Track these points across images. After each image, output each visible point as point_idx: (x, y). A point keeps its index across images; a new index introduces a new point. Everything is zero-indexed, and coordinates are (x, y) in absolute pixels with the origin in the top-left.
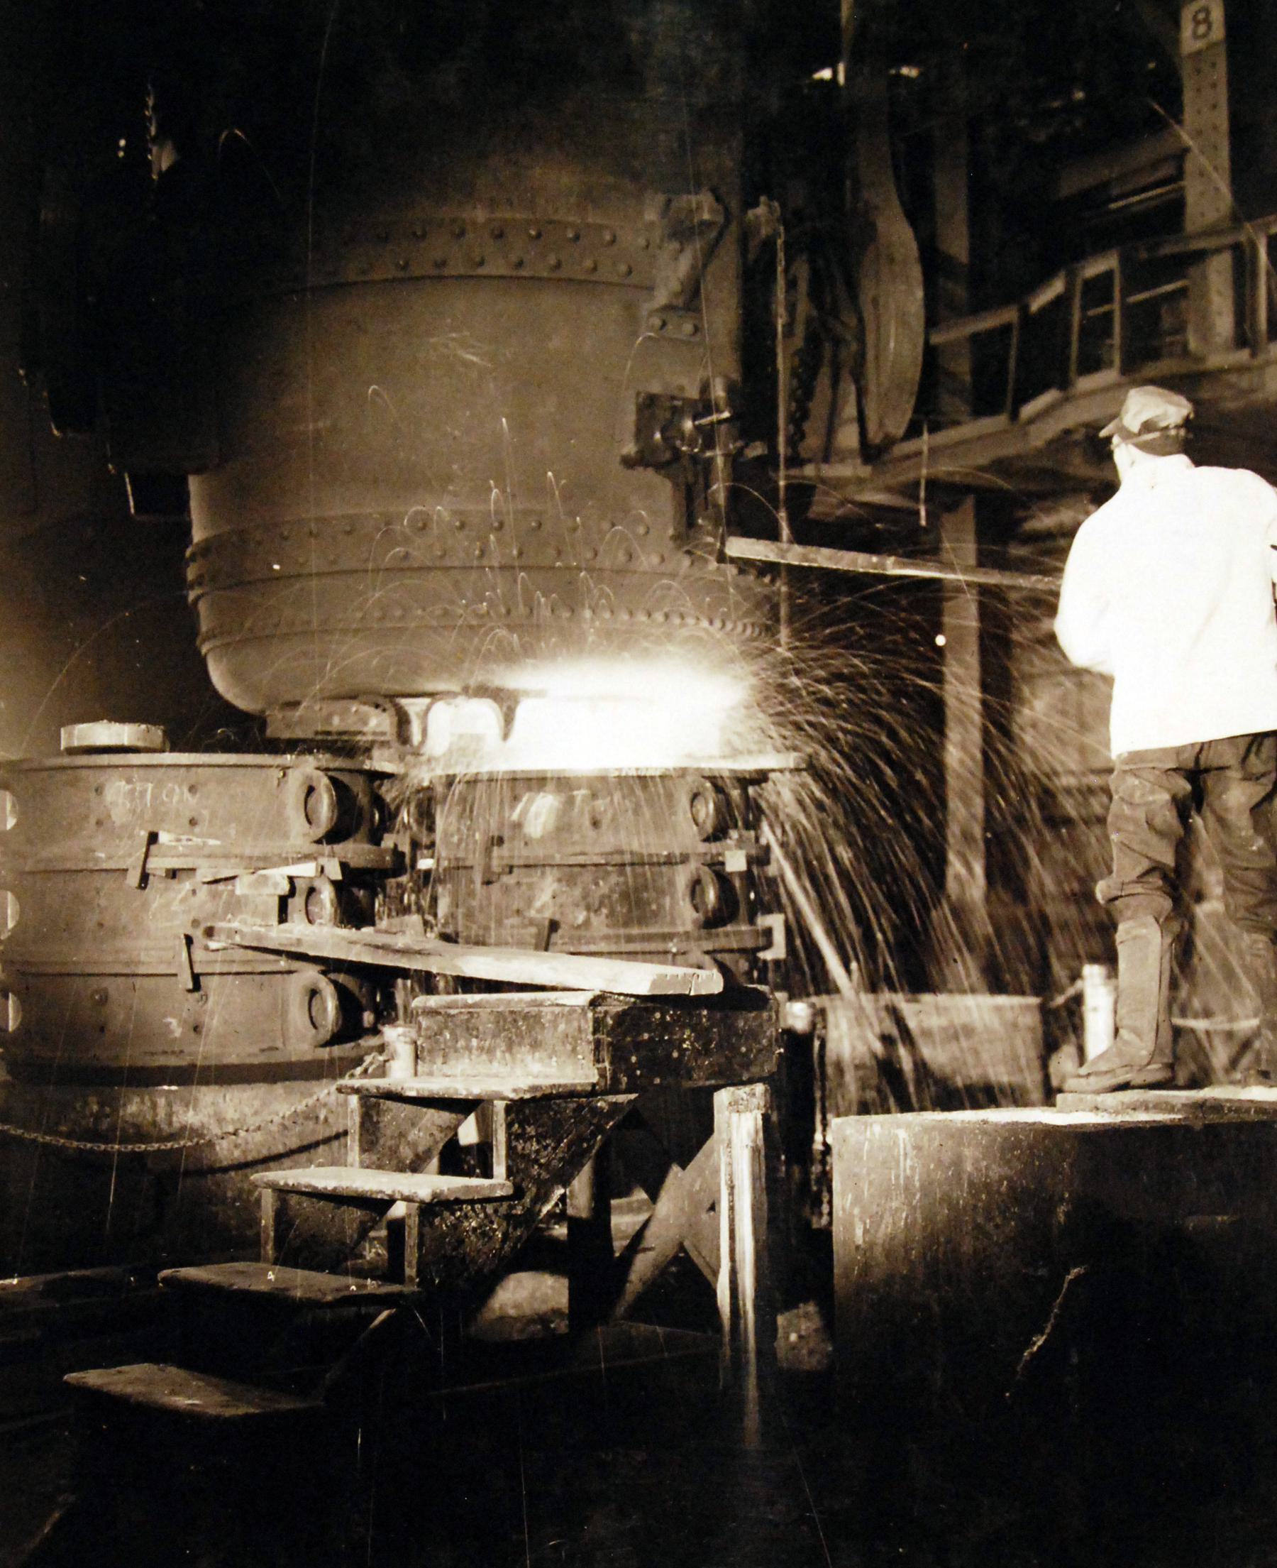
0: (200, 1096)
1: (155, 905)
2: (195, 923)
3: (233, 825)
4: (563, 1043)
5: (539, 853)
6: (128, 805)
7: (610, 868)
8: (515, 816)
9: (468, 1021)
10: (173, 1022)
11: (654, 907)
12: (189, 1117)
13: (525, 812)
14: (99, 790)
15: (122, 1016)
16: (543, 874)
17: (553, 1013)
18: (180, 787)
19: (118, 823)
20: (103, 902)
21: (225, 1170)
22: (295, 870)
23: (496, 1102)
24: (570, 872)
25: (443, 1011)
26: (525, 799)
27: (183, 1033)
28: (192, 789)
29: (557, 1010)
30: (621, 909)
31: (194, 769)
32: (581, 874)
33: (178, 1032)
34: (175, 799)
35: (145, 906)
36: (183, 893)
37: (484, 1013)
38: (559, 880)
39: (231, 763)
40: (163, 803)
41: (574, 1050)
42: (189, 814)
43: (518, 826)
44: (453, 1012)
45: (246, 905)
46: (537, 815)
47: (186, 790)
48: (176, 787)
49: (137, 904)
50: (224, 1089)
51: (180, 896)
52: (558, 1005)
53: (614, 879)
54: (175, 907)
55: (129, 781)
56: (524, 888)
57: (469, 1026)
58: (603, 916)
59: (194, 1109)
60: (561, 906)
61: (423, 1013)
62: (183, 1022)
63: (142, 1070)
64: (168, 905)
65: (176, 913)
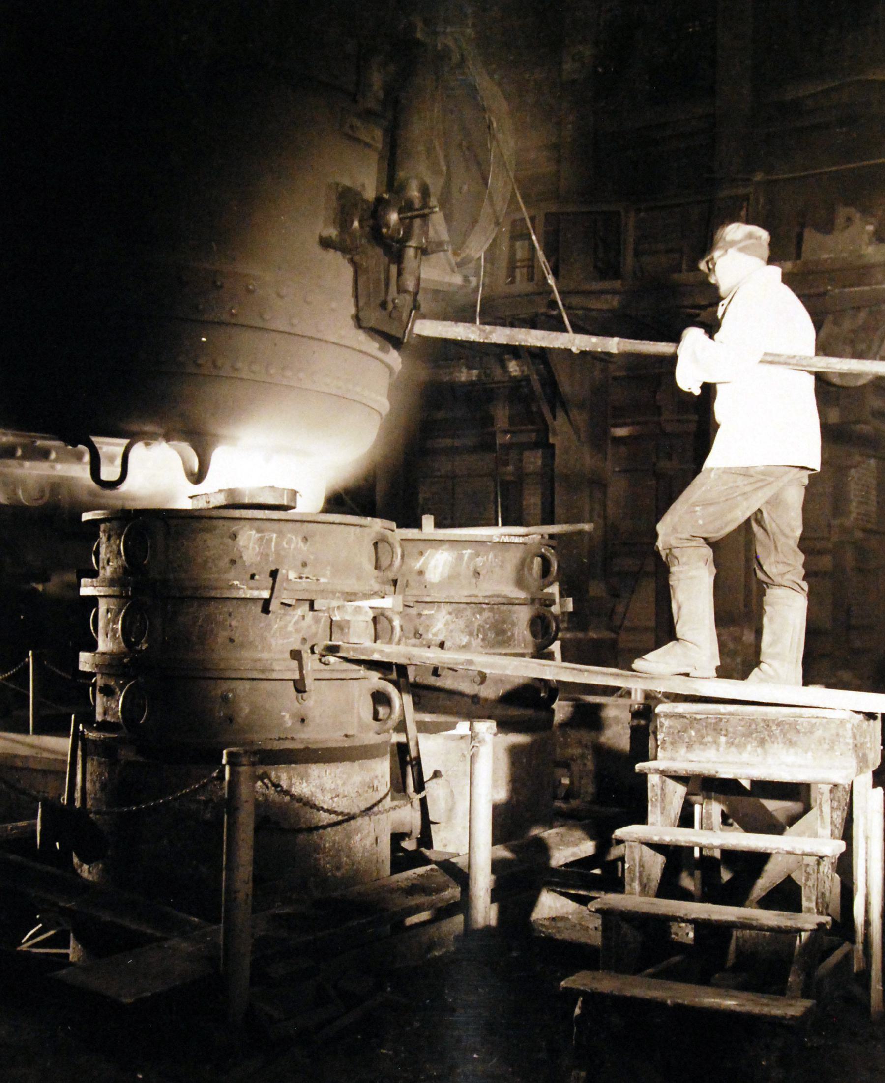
0: (310, 771)
1: (276, 626)
2: (304, 640)
3: (329, 568)
5: (436, 596)
6: (257, 549)
7: (484, 606)
8: (418, 565)
9: (716, 723)
10: (287, 716)
11: (509, 634)
12: (301, 788)
13: (426, 564)
14: (234, 536)
15: (247, 711)
16: (439, 607)
17: (809, 722)
18: (296, 537)
20: (234, 623)
21: (324, 827)
22: (378, 603)
24: (457, 607)
25: (688, 716)
26: (427, 555)
27: (293, 724)
28: (305, 539)
29: (814, 721)
30: (491, 635)
31: (306, 524)
32: (465, 609)
33: (289, 723)
34: (292, 546)
35: (268, 626)
37: (733, 720)
40: (284, 549)
42: (300, 559)
44: (698, 717)
46: (435, 567)
48: (294, 537)
50: (326, 766)
51: (295, 619)
53: (486, 614)
54: (290, 628)
55: (259, 530)
56: (423, 618)
57: (717, 727)
58: (479, 640)
59: (306, 782)
60: (452, 631)
62: (293, 716)
64: (286, 626)
65: (290, 632)
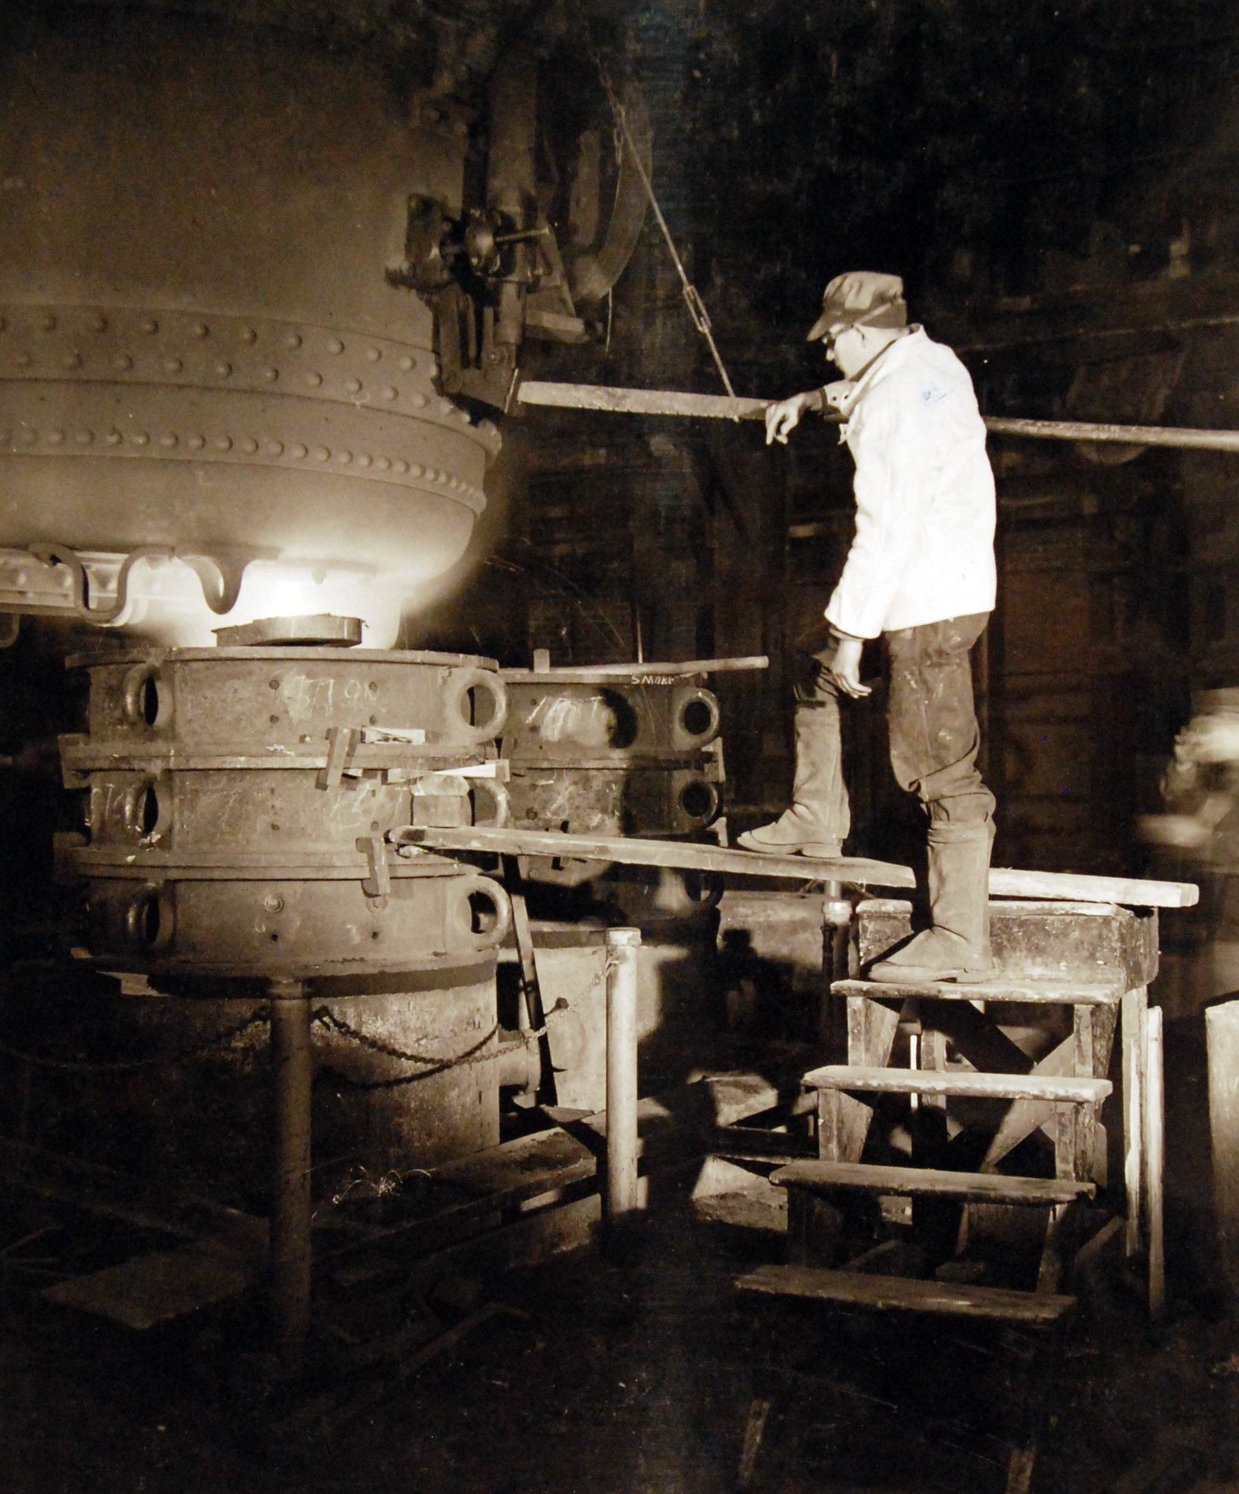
0: (387, 1005)
2: (375, 825)
4: (1077, 949)
12: (376, 1028)
13: (542, 714)
17: (1063, 921)
18: (362, 684)
19: (295, 720)
21: (409, 1080)
23: (1076, 1006)
28: (373, 685)
29: (1068, 919)
36: (363, 795)
38: (575, 783)
39: (419, 660)
41: (1092, 957)
43: (534, 729)
45: (436, 806)
46: (554, 720)
47: (366, 686)
49: (317, 805)
51: (360, 798)
52: (1073, 914)
54: (356, 808)
55: (309, 676)
60: (577, 808)
61: (869, 917)
63: (334, 979)
64: (350, 806)
